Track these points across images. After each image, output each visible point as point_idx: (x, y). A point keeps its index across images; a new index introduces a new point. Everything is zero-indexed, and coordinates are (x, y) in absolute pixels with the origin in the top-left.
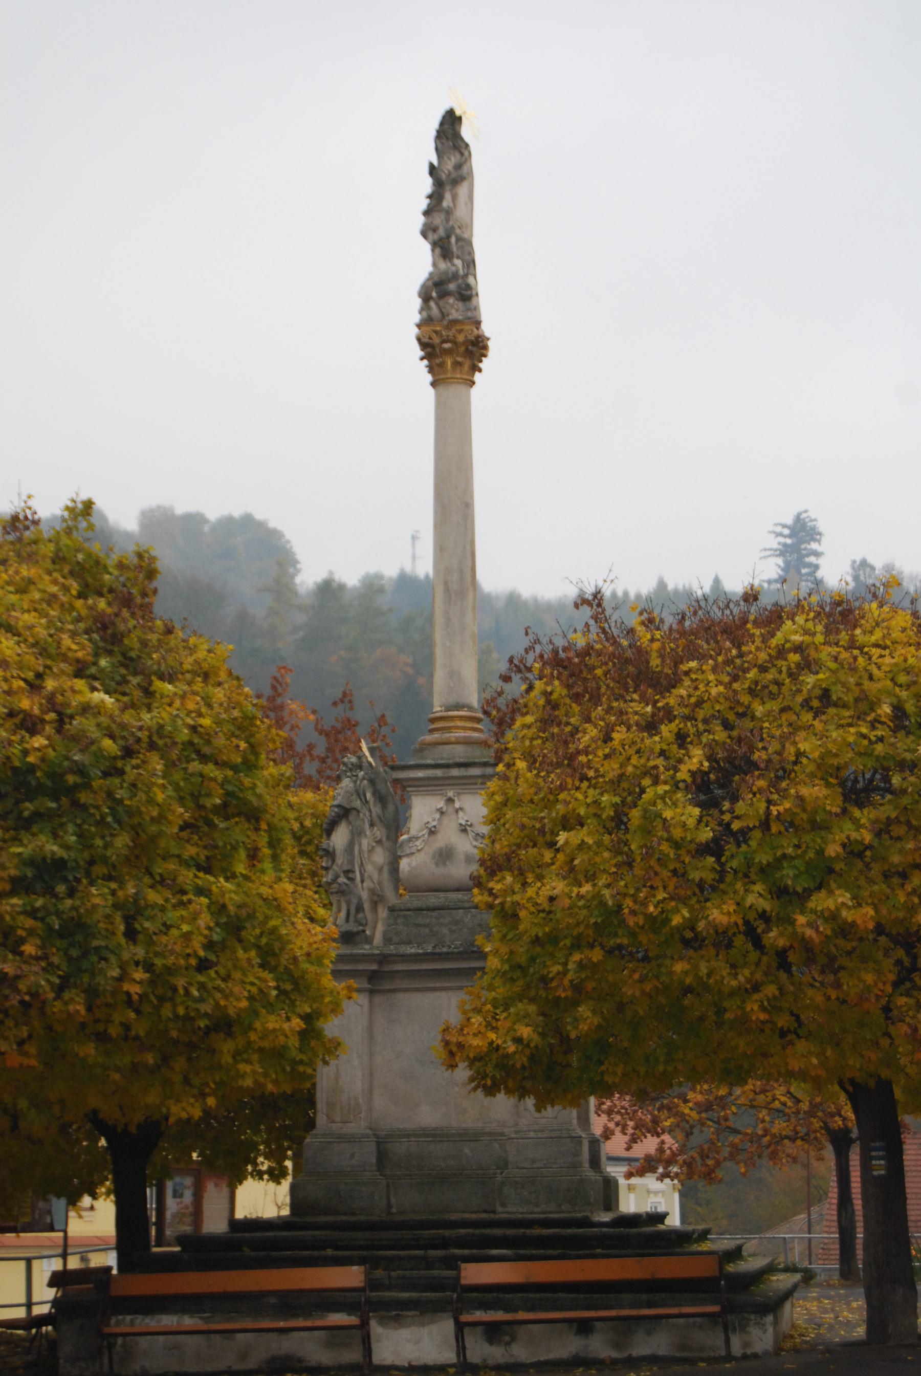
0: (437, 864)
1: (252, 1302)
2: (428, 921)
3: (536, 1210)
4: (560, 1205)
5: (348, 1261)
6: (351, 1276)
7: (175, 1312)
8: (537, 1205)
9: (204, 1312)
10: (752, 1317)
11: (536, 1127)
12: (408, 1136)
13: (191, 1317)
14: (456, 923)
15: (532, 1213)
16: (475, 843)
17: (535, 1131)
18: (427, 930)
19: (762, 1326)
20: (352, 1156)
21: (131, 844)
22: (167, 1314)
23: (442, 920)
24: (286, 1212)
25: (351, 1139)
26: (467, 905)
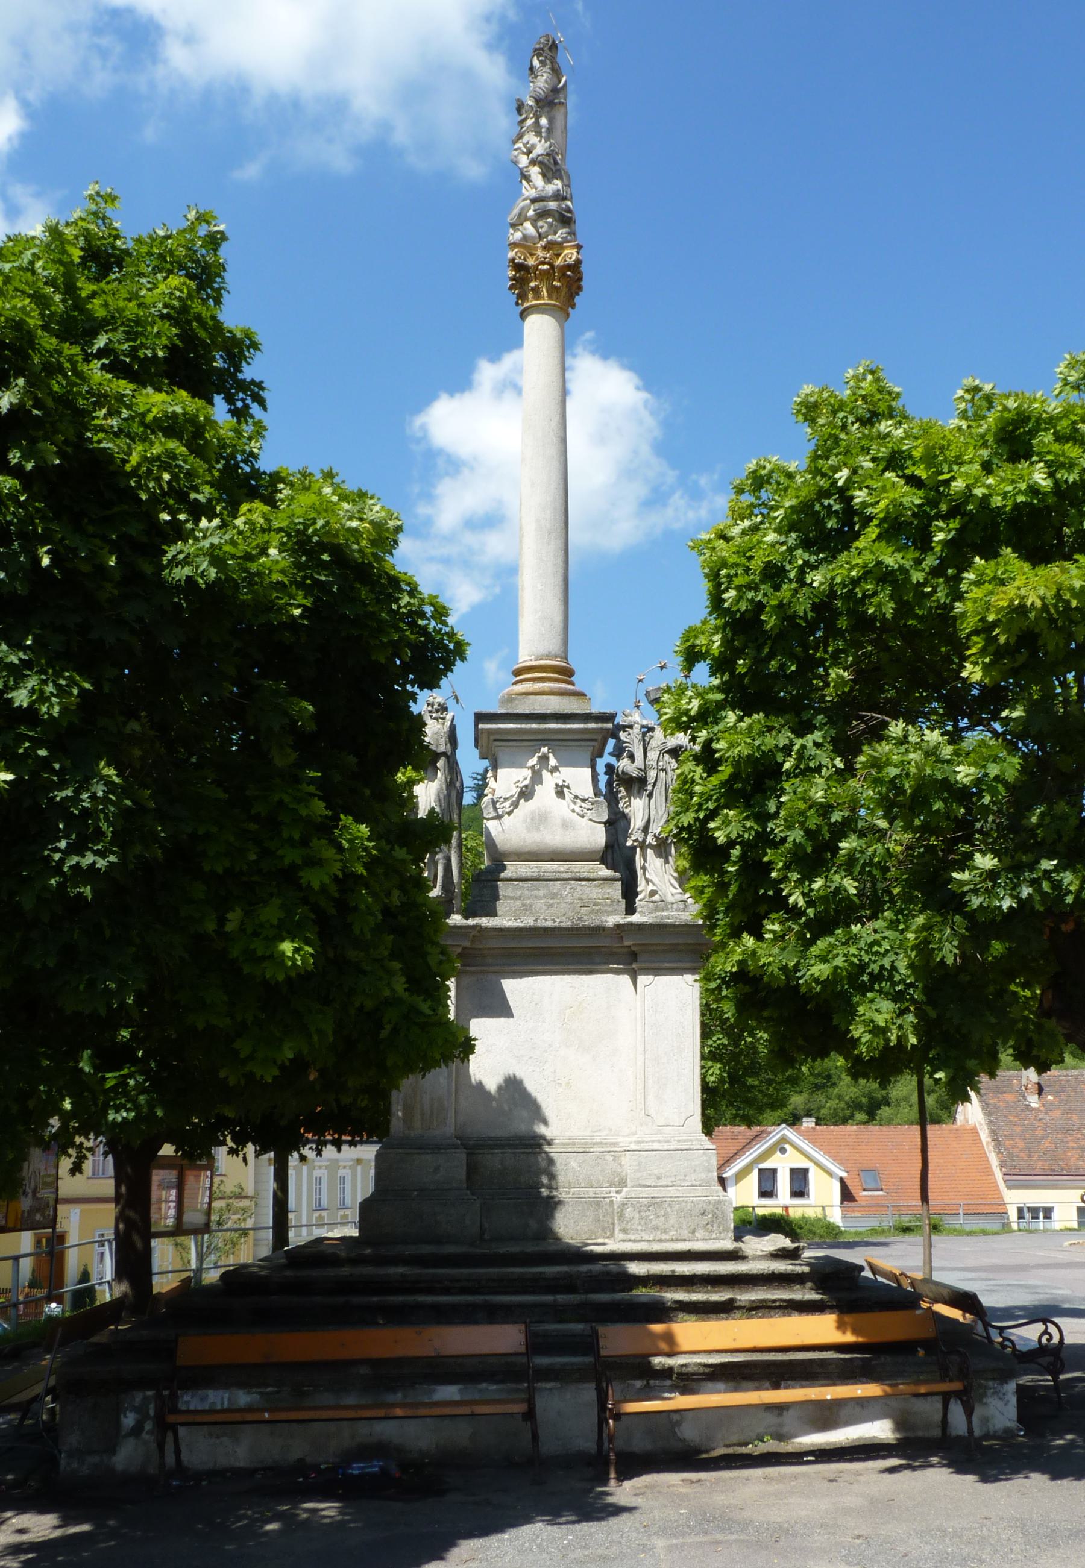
0: (528, 829)
1: (337, 1373)
2: (519, 893)
3: (664, 1237)
4: (693, 1232)
5: (494, 1315)
6: (504, 1339)
7: (227, 1386)
8: (665, 1231)
9: (268, 1386)
10: (991, 1383)
11: (659, 1137)
12: (501, 1146)
13: (249, 1393)
14: (554, 896)
15: (660, 1241)
16: (572, 806)
17: (659, 1141)
18: (518, 903)
19: (1002, 1396)
20: (437, 1169)
21: (149, 417)
22: (216, 1388)
23: (535, 892)
24: (155, 1291)
25: (436, 1147)
26: (565, 876)
